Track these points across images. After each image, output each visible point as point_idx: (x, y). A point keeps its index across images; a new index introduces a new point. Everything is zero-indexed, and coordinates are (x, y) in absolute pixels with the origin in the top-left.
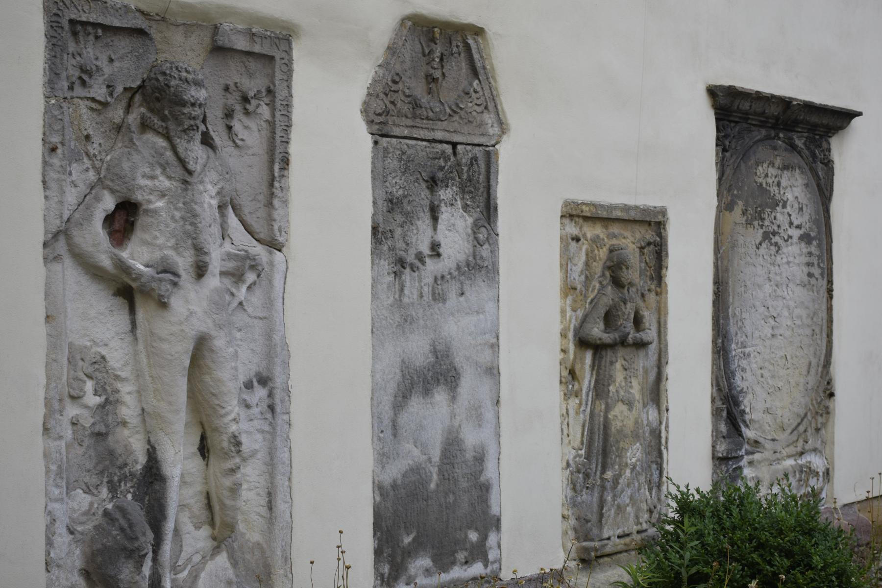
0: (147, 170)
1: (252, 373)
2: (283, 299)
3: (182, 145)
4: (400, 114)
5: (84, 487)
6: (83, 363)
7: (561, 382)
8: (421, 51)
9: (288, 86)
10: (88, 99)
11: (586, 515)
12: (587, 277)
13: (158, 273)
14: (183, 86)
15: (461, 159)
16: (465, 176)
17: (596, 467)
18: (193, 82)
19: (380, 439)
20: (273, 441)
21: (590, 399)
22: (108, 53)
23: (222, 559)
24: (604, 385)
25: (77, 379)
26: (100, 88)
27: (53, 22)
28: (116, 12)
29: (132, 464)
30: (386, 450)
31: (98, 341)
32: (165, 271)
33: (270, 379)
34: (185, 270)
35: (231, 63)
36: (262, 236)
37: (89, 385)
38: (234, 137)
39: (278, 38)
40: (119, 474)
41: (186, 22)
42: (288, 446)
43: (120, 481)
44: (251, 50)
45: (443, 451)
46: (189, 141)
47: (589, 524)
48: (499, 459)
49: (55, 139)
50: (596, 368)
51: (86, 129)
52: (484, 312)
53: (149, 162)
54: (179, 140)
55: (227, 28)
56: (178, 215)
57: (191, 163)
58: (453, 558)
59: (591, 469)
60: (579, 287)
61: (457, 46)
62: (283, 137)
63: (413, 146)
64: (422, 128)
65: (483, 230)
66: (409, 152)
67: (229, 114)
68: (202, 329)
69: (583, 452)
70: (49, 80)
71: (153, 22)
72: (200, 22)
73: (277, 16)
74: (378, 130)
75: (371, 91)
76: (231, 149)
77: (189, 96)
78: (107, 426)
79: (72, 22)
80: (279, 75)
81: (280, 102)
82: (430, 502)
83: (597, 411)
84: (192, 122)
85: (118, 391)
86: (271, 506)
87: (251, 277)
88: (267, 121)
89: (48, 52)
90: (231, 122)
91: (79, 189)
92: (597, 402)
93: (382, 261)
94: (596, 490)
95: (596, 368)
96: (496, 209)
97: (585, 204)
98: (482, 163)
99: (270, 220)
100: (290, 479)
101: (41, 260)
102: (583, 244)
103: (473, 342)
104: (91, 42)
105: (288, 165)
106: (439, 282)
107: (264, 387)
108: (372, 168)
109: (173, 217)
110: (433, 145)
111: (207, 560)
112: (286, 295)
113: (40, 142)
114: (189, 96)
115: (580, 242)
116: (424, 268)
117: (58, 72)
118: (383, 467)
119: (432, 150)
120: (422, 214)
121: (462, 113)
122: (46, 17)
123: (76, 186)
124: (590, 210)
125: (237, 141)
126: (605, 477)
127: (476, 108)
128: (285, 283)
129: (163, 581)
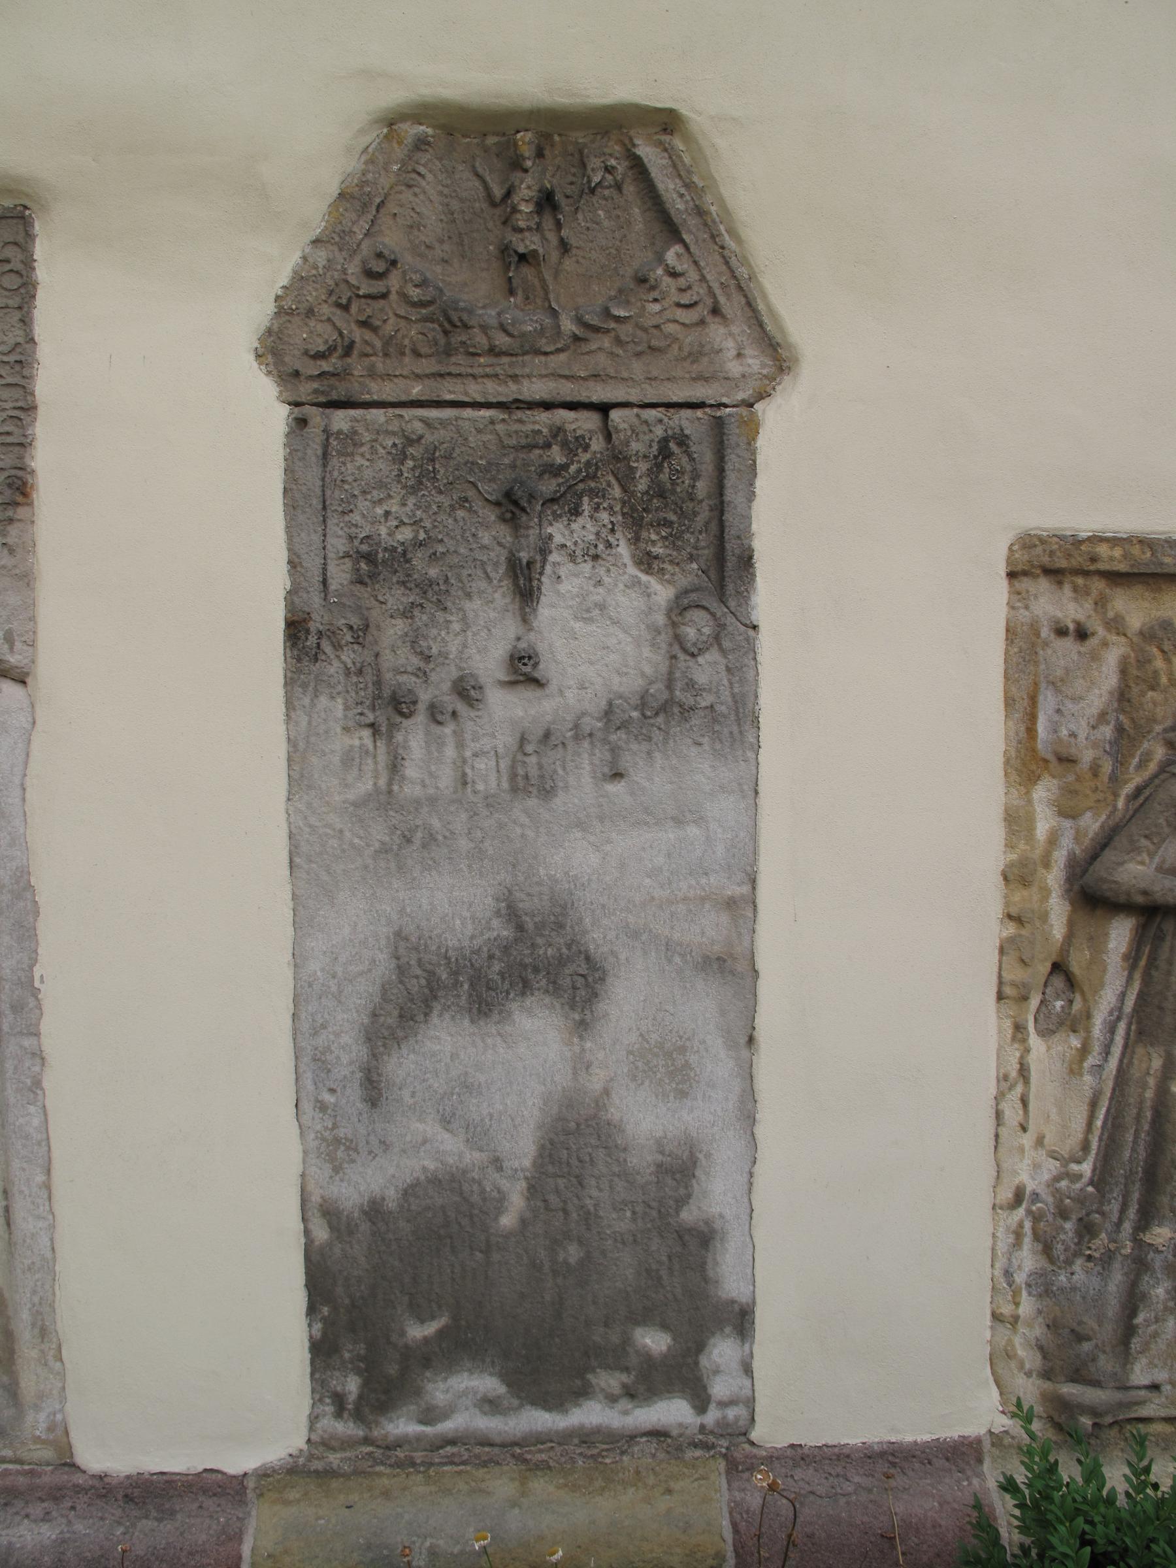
4: (392, 347)
7: (1000, 997)
8: (482, 193)
9: (22, 321)
11: (1080, 1323)
12: (1120, 730)
15: (627, 444)
16: (642, 485)
17: (1123, 1210)
19: (322, 1107)
21: (1119, 1039)
24: (1161, 1008)
30: (341, 1132)
45: (543, 1147)
47: (1086, 1346)
48: (751, 1175)
50: (1143, 963)
52: (700, 820)
58: (578, 1382)
59: (1103, 1214)
60: (1087, 756)
61: (609, 170)
63: (443, 423)
64: (474, 376)
65: (699, 616)
66: (429, 438)
69: (1086, 1168)
74: (316, 391)
75: (287, 303)
82: (496, 1257)
83: (1136, 1073)
92: (1140, 1050)
94: (1117, 1265)
95: (1143, 963)
96: (747, 561)
97: (1102, 540)
98: (704, 453)
102: (1105, 644)
103: (658, 893)
105: (25, 495)
106: (529, 749)
108: (285, 482)
110: (519, 414)
115: (1093, 642)
116: (473, 714)
118: (337, 1170)
119: (517, 427)
120: (483, 584)
121: (625, 331)
124: (1125, 556)
126: (1148, 1238)
127: (682, 315)
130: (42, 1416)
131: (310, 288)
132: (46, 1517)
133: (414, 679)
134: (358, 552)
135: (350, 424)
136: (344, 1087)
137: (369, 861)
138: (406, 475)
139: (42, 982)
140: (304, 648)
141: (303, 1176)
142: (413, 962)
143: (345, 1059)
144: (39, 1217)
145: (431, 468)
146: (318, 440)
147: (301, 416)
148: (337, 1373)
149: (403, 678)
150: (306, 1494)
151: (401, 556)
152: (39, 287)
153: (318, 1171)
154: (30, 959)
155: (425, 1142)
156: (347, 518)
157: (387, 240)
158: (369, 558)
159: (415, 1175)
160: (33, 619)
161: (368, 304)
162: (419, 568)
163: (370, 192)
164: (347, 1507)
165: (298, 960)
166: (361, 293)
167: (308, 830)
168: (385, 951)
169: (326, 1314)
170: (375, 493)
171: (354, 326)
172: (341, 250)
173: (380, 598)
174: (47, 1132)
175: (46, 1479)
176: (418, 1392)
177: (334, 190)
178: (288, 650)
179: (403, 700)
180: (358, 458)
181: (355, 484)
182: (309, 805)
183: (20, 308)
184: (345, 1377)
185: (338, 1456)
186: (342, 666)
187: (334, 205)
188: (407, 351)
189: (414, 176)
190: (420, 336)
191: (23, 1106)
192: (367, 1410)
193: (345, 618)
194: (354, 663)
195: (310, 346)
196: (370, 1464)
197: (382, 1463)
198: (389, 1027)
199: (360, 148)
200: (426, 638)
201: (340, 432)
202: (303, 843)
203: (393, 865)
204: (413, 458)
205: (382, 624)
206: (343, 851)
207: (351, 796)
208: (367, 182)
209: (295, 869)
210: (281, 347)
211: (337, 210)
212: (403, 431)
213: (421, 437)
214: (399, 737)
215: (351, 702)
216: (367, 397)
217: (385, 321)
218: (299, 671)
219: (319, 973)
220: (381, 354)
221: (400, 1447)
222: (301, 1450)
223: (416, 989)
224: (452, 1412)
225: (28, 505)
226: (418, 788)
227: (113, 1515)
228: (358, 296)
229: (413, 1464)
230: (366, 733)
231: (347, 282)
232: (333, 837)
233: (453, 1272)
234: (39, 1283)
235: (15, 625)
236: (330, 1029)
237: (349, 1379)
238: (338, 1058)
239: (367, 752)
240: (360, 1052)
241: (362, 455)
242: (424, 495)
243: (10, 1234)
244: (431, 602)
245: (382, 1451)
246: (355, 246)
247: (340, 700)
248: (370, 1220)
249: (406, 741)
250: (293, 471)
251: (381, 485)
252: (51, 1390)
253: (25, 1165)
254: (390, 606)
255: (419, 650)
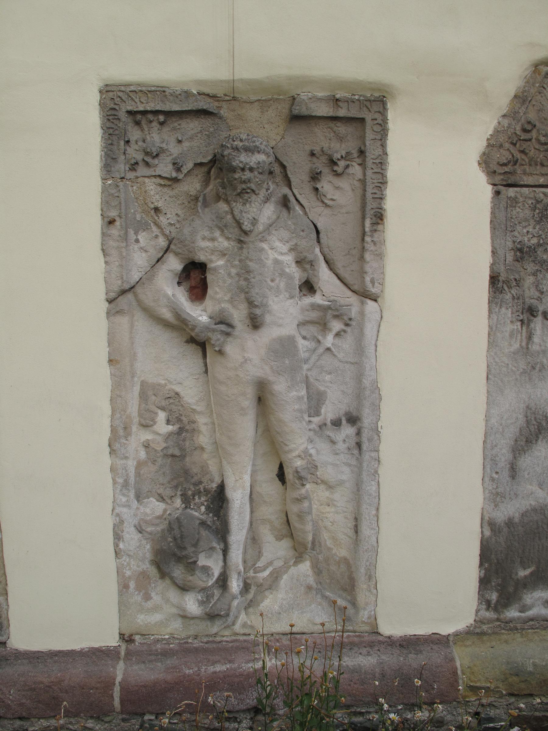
0: (207, 233)
1: (342, 412)
2: (376, 346)
3: (238, 208)
4: (533, 162)
5: (157, 496)
6: (155, 398)
9: (382, 145)
10: (155, 176)
13: (216, 324)
14: (233, 154)
18: (244, 149)
19: (493, 479)
20: (360, 474)
22: (176, 136)
23: (305, 567)
25: (148, 410)
26: (166, 166)
27: (110, 115)
28: (175, 98)
29: (207, 483)
30: (499, 490)
31: (172, 380)
32: (221, 323)
33: (359, 419)
34: (240, 321)
35: (316, 130)
36: (356, 288)
37: (162, 416)
38: (323, 198)
39: (370, 101)
40: (193, 489)
41: (260, 98)
42: (377, 481)
43: (194, 495)
44: (334, 115)
46: (244, 204)
49: (113, 214)
51: (152, 203)
53: (208, 227)
54: (234, 204)
55: (305, 98)
56: (234, 271)
57: (246, 223)
62: (375, 193)
67: (315, 177)
68: (258, 374)
70: (104, 165)
71: (224, 103)
72: (275, 97)
73: (361, 79)
74: (502, 180)
75: (492, 142)
76: (321, 209)
77: (238, 162)
78: (182, 449)
79: (129, 113)
80: (369, 135)
81: (372, 161)
84: (244, 186)
85: (194, 422)
86: (357, 530)
87: (336, 326)
88: (360, 180)
89: (104, 141)
90: (316, 184)
91: (149, 254)
93: (503, 310)
99: (363, 272)
100: (378, 509)
101: (104, 315)
104: (156, 129)
105: (382, 220)
107: (353, 426)
108: (491, 218)
109: (229, 274)
111: (291, 566)
112: (379, 343)
113: (99, 217)
114: (238, 162)
117: (114, 157)
118: (496, 506)
122: (102, 112)
123: (146, 251)
125: (326, 201)
128: (378, 331)
129: (229, 580)
130: (366, 613)
131: (501, 136)
132: (369, 654)
133: (536, 301)
134: (517, 248)
135: (515, 194)
136: (502, 471)
137: (518, 377)
138: (536, 216)
139: (382, 428)
140: (497, 288)
141: (483, 509)
142: (533, 419)
143: (503, 460)
144: (372, 529)
145: (545, 213)
146: (505, 200)
147: (497, 190)
148: (489, 592)
149: (532, 301)
150: (473, 643)
151: (532, 250)
152: (389, 131)
153: (488, 506)
154: (376, 419)
155: (532, 494)
156: (512, 234)
157: (530, 116)
158: (520, 250)
159: (527, 507)
160: (383, 273)
161: (524, 143)
162: (540, 255)
163: (526, 95)
164: (492, 647)
165: (487, 418)
166: (521, 138)
167: (494, 364)
168: (522, 414)
169: (487, 566)
170: (524, 223)
171: (518, 153)
172: (514, 120)
173: (525, 267)
174: (379, 493)
175: (366, 639)
176: (520, 599)
177: (512, 94)
178: (491, 289)
179: (535, 310)
180: (517, 208)
181: (516, 219)
182: (496, 354)
183: (381, 140)
184: (492, 593)
185: (486, 626)
186: (511, 295)
187: (512, 101)
188: (539, 164)
189: (542, 89)
190: (544, 158)
191: (369, 481)
192: (499, 607)
193: (514, 275)
194: (516, 294)
195: (500, 160)
196: (499, 629)
197: (504, 629)
198: (522, 446)
199: (524, 76)
200: (542, 284)
201: (511, 197)
202: (492, 369)
203: (527, 378)
204: (539, 209)
205: (525, 278)
206: (508, 373)
207: (512, 349)
208: (525, 91)
209: (489, 380)
210: (488, 160)
211: (513, 103)
212: (535, 197)
213: (542, 200)
214: (532, 325)
215: (514, 311)
216: (522, 183)
217: (530, 151)
218: (495, 297)
219: (495, 424)
220: (528, 165)
221: (511, 622)
222: (472, 624)
223: (533, 430)
224: (533, 607)
225: (382, 224)
226: (538, 346)
227: (396, 652)
228: (520, 140)
229: (517, 629)
230: (519, 324)
231: (515, 133)
232: (504, 367)
233: (538, 548)
234: (370, 557)
235: (375, 276)
236: (498, 447)
237: (493, 594)
238: (500, 459)
239: (519, 332)
240: (510, 456)
241: (519, 207)
242: (543, 225)
243: (357, 536)
244: (544, 269)
245: (504, 624)
246: (520, 118)
247: (510, 310)
248: (508, 527)
249: (535, 327)
250: (494, 213)
251: (526, 220)
252: (371, 601)
253: (368, 507)
254: (528, 271)
255: (539, 289)
